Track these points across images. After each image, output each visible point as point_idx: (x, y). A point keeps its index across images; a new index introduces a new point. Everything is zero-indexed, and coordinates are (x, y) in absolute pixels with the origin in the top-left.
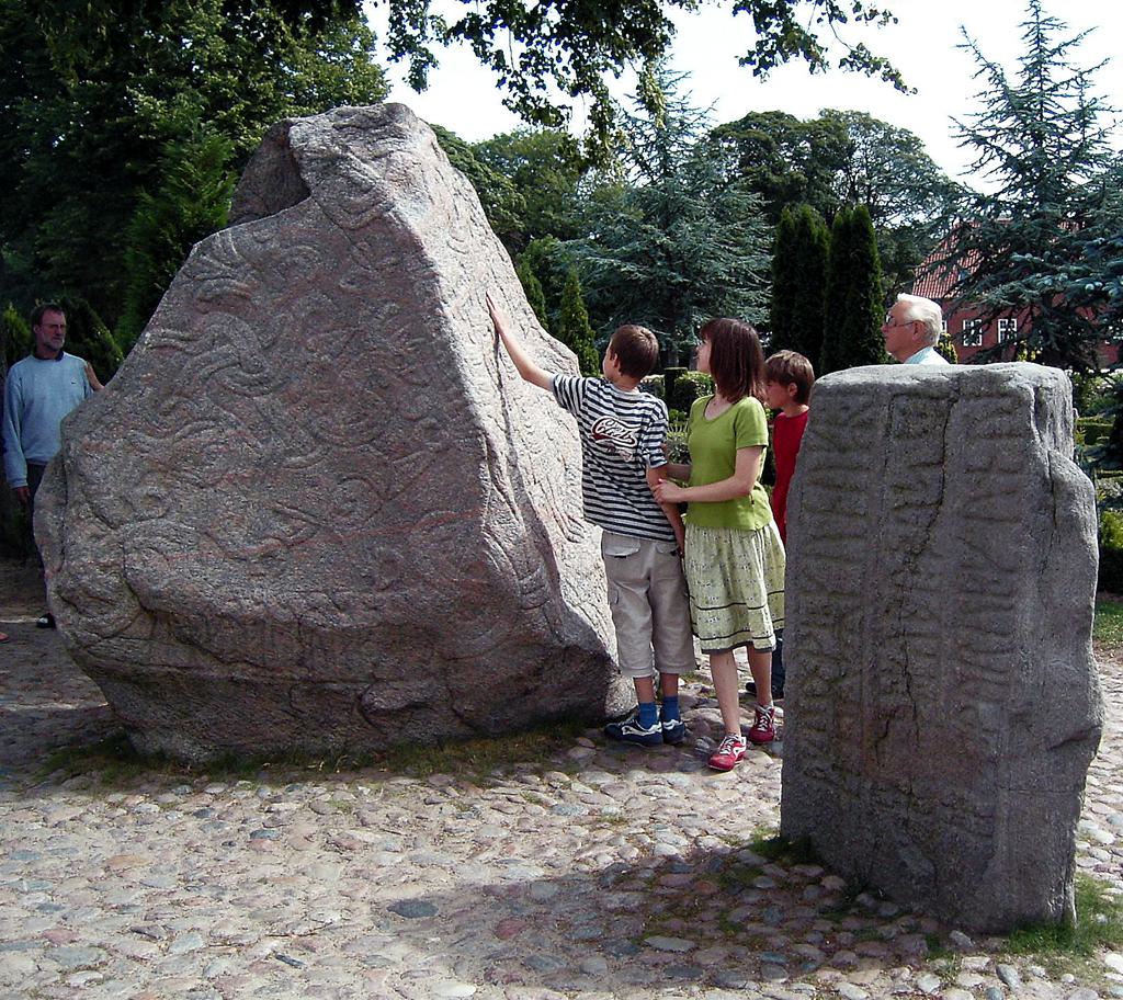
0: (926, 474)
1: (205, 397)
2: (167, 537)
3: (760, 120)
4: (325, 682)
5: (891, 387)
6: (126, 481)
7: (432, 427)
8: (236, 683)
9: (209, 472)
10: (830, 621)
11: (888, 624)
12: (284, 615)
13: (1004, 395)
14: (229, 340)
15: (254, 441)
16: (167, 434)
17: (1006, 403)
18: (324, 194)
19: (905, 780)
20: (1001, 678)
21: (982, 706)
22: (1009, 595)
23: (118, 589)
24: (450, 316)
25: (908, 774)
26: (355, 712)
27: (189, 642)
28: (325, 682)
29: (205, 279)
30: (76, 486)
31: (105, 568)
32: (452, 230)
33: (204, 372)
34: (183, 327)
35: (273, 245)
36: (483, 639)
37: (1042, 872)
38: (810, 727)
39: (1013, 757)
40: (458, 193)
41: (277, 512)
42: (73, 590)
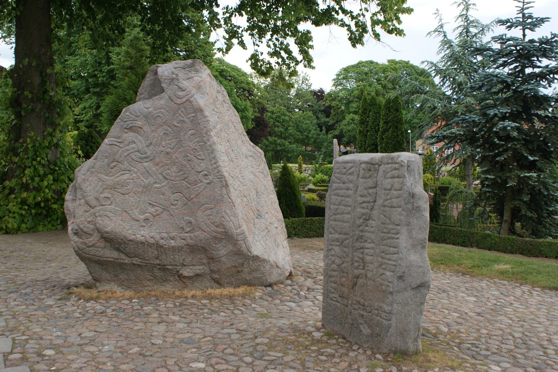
0: (370, 191)
1: (126, 163)
2: (111, 212)
3: (364, 64)
4: (166, 265)
5: (359, 161)
6: (97, 192)
7: (206, 175)
8: (134, 264)
9: (127, 189)
10: (338, 243)
11: (357, 245)
12: (152, 241)
13: (396, 163)
14: (135, 143)
15: (143, 178)
16: (112, 176)
17: (397, 166)
18: (169, 92)
19: (362, 301)
20: (394, 263)
21: (388, 273)
22: (397, 234)
23: (93, 230)
24: (213, 136)
25: (363, 298)
26: (176, 276)
27: (118, 250)
28: (166, 265)
29: (126, 121)
30: (79, 193)
31: (89, 222)
32: (215, 105)
33: (125, 154)
34: (118, 138)
35: (150, 110)
36: (222, 251)
37: (408, 334)
38: (331, 282)
39: (398, 292)
40: (218, 92)
41: (150, 204)
42: (77, 230)
